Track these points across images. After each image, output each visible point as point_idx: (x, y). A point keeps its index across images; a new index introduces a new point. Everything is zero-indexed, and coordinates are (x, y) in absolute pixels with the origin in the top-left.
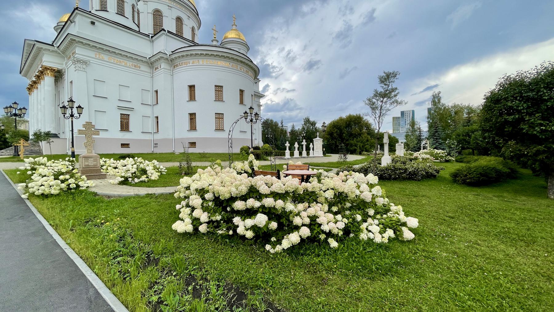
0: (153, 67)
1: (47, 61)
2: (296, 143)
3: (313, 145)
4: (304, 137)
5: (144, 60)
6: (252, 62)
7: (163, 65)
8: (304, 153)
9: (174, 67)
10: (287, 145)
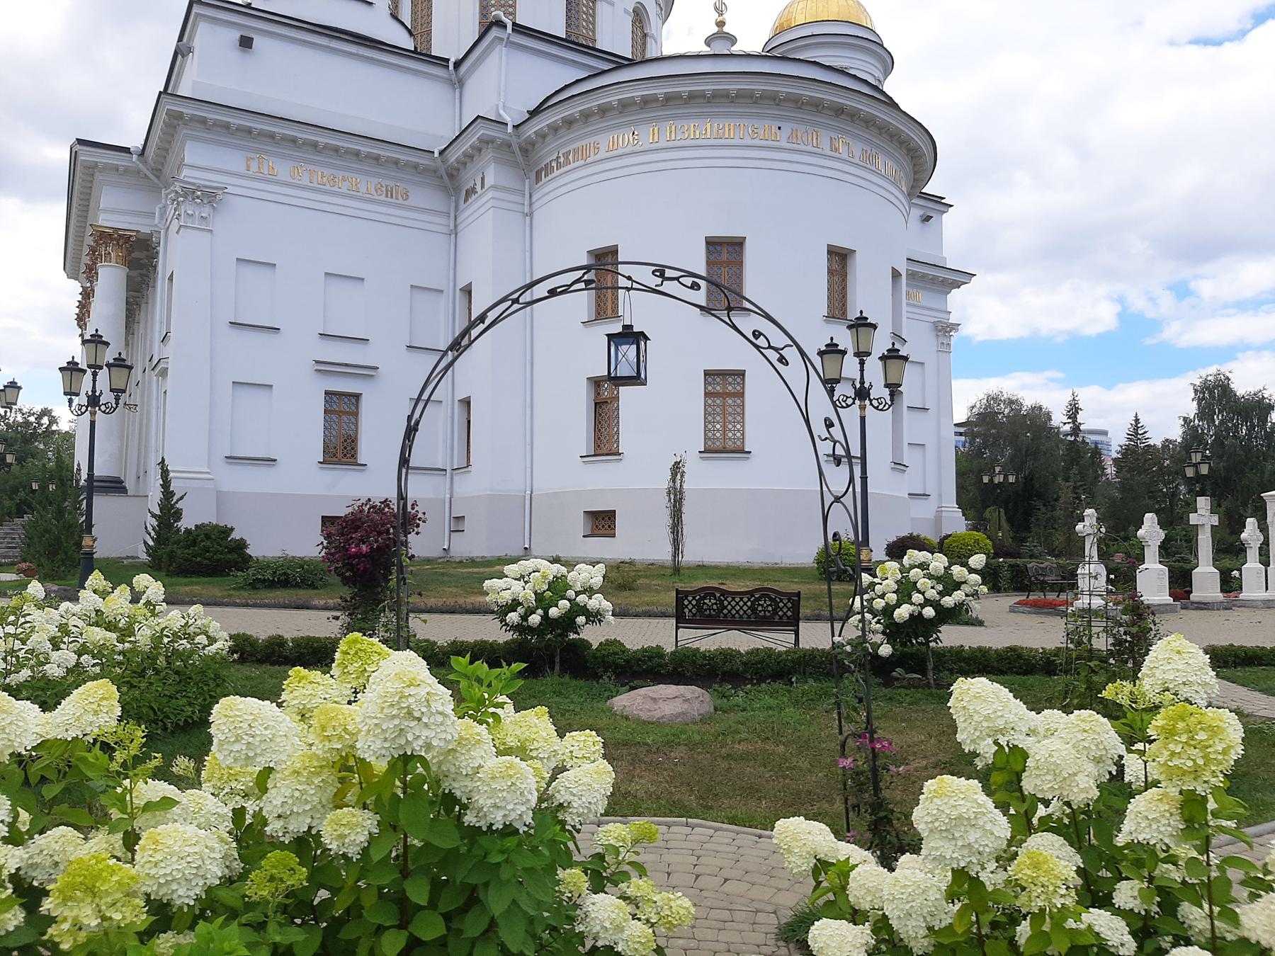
0: (457, 190)
1: (113, 211)
2: (1150, 518)
3: (1264, 528)
4: (1200, 485)
5: (422, 160)
6: (894, 105)
7: (492, 173)
8: (1206, 576)
9: (538, 179)
10: (1088, 524)
